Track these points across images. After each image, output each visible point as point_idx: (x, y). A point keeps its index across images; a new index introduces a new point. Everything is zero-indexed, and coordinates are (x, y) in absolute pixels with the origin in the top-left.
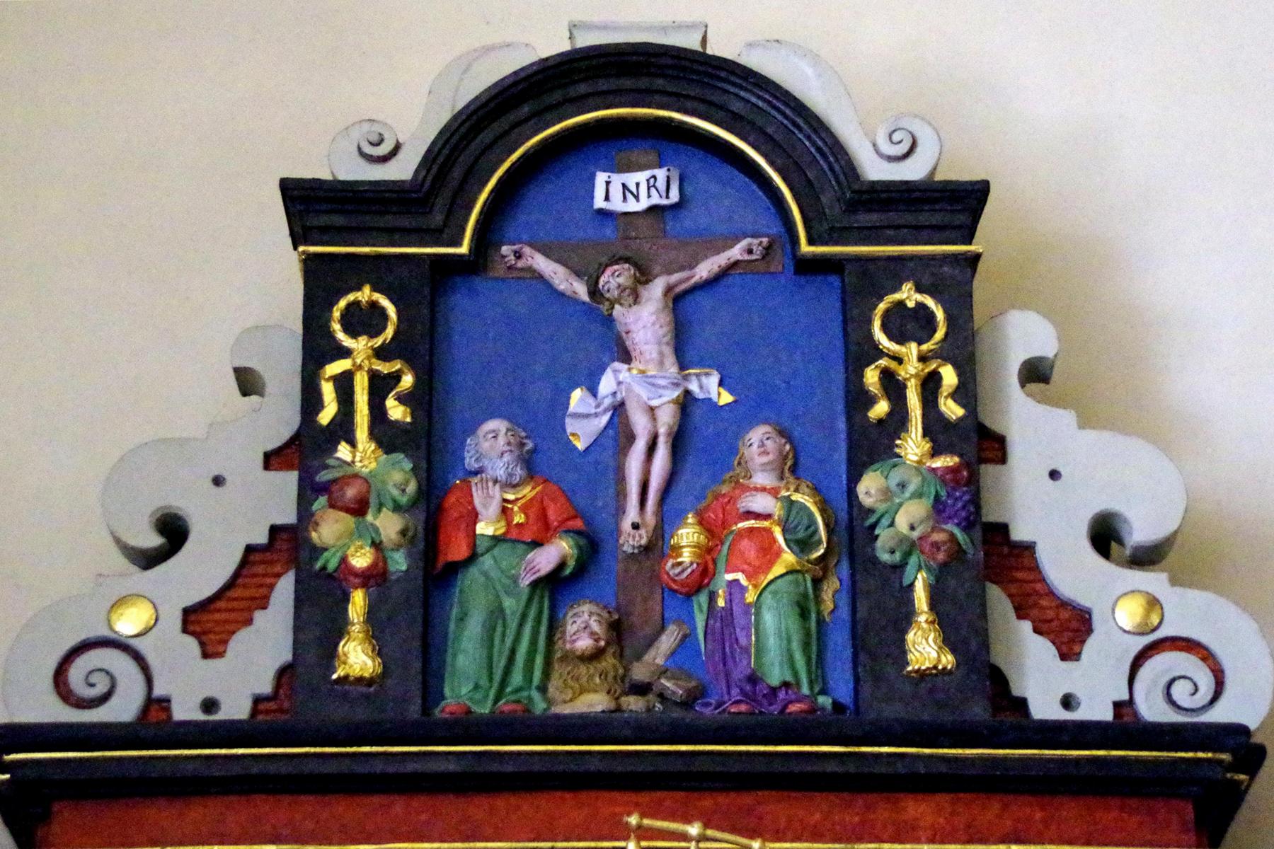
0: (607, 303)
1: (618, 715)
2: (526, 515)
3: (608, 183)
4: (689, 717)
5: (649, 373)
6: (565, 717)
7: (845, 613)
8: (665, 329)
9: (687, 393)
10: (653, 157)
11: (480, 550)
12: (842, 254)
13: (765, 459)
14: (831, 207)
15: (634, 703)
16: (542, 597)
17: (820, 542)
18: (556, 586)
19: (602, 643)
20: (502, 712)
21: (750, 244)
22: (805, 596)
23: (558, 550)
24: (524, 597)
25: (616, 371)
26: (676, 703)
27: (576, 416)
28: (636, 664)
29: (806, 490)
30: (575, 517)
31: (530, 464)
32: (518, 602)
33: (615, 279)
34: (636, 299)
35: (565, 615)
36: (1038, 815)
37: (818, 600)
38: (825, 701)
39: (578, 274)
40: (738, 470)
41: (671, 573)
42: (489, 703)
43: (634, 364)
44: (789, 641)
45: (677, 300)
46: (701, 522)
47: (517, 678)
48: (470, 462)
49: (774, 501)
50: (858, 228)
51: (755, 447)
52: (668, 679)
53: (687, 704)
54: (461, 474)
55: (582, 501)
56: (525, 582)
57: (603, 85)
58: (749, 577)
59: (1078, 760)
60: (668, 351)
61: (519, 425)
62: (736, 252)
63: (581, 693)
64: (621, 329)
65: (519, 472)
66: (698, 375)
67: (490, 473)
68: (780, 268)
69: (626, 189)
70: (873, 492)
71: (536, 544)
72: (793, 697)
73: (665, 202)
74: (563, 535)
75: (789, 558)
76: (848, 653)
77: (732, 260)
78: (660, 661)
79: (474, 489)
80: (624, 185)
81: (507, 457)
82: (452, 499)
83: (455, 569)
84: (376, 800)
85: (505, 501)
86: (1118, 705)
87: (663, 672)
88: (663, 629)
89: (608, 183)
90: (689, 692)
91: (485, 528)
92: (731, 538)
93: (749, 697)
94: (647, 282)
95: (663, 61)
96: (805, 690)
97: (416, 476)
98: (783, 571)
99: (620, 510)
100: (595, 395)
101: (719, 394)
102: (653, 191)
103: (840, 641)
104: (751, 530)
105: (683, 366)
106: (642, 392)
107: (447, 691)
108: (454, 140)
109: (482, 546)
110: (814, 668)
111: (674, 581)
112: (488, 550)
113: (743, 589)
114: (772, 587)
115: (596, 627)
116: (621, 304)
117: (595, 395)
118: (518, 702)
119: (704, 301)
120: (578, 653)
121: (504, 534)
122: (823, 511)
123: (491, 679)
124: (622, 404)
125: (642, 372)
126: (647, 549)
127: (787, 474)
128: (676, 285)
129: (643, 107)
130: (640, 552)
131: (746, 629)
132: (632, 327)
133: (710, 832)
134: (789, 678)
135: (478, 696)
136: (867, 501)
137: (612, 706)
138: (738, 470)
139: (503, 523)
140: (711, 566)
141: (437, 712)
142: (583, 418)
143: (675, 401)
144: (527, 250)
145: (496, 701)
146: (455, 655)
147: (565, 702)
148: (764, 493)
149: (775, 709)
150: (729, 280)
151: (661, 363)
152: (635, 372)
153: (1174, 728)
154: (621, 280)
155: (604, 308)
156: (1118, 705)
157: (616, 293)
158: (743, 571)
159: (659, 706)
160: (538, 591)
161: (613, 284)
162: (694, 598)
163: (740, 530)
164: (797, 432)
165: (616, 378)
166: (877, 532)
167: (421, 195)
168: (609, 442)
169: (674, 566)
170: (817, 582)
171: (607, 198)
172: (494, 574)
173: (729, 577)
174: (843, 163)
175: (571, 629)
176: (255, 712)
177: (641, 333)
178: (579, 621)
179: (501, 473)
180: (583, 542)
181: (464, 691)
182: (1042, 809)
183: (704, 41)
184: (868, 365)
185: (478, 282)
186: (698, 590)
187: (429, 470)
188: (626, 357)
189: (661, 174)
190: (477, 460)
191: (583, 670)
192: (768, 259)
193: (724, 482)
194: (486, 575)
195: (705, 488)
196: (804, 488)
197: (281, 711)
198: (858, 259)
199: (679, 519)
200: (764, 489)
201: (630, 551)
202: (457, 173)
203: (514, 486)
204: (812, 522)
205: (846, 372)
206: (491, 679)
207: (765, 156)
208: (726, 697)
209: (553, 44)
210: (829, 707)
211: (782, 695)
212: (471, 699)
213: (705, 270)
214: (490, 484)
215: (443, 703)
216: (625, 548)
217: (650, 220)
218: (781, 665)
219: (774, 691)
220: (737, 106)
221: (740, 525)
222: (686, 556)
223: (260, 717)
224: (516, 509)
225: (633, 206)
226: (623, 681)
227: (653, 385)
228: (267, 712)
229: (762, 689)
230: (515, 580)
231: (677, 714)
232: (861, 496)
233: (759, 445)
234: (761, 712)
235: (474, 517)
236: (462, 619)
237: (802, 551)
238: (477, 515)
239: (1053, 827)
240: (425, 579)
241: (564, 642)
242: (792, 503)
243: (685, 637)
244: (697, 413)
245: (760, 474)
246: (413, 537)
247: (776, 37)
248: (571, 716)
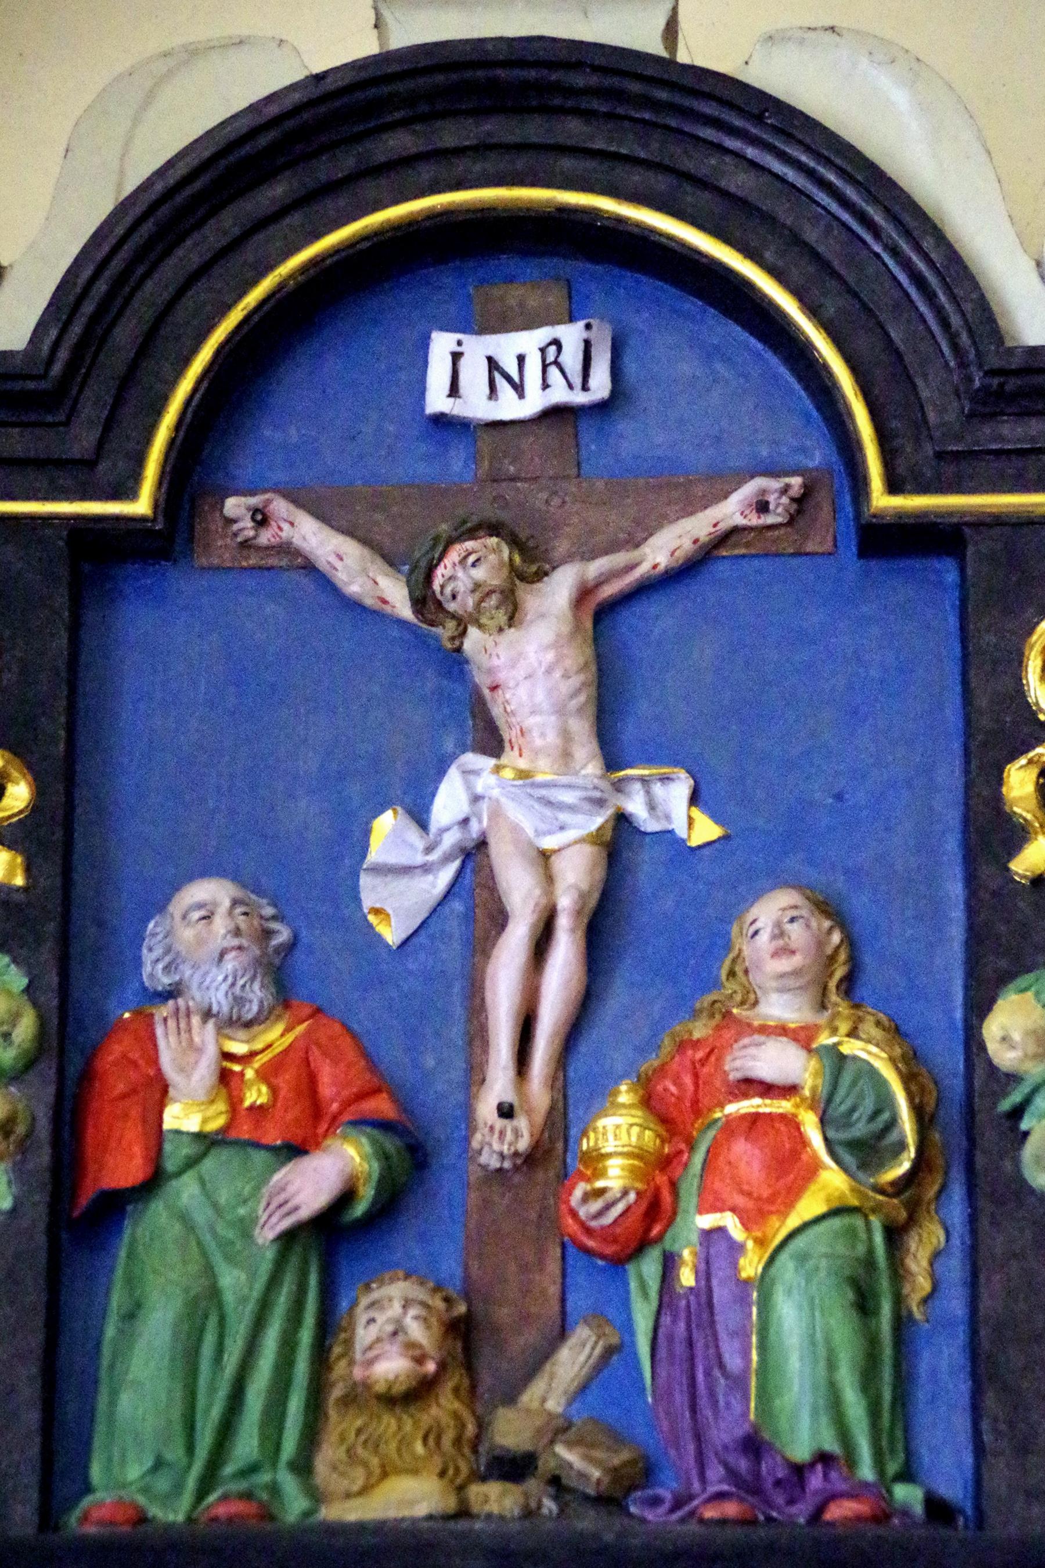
0: (451, 624)
1: (462, 1525)
2: (274, 1091)
3: (456, 356)
5: (540, 778)
7: (956, 1304)
8: (576, 681)
9: (622, 819)
10: (556, 297)
11: (170, 1165)
12: (962, 512)
13: (785, 965)
14: (942, 410)
15: (497, 1499)
16: (305, 1262)
17: (901, 1146)
18: (335, 1242)
19: (431, 1367)
20: (215, 1519)
21: (764, 492)
22: (869, 1262)
23: (341, 1163)
24: (265, 1268)
25: (467, 773)
26: (586, 1497)
27: (381, 870)
28: (501, 1412)
29: (876, 1033)
30: (376, 1091)
31: (282, 975)
32: (252, 1276)
33: (468, 571)
34: (514, 617)
35: (354, 1304)
37: (898, 1272)
38: (908, 1495)
39: (391, 561)
40: (730, 987)
41: (582, 1213)
43: (510, 757)
44: (832, 1365)
45: (603, 616)
46: (648, 1101)
47: (247, 1444)
48: (154, 972)
49: (802, 1054)
50: (998, 453)
51: (764, 937)
52: (570, 1445)
53: (609, 1501)
54: (130, 994)
55: (392, 1054)
56: (267, 1234)
57: (450, 134)
58: (746, 1225)
60: (582, 728)
61: (258, 891)
62: (732, 510)
63: (385, 1475)
64: (482, 681)
65: (257, 995)
66: (644, 781)
67: (195, 997)
68: (828, 546)
69: (499, 369)
70: (1017, 1036)
71: (294, 1150)
72: (843, 1487)
73: (579, 398)
74: (351, 1131)
75: (833, 1181)
76: (964, 1387)
77: (723, 526)
78: (555, 1405)
79: (159, 1031)
80: (492, 364)
81: (230, 964)
82: (114, 1051)
83: (115, 1207)
85: (228, 1056)
87: (561, 1429)
88: (562, 1333)
89: (456, 356)
90: (615, 1473)
91: (183, 1117)
92: (711, 1134)
93: (749, 1487)
94: (541, 575)
95: (579, 80)
96: (866, 1472)
97: (35, 1004)
98: (820, 1209)
99: (475, 1075)
100: (423, 825)
101: (691, 821)
102: (554, 372)
103: (943, 1361)
104: (755, 1118)
105: (612, 762)
106: (523, 817)
107: (96, 1472)
108: (116, 265)
109: (174, 1155)
110: (886, 1416)
111: (589, 1231)
112: (191, 1163)
113: (736, 1249)
114: (799, 1243)
115: (416, 1331)
116: (480, 626)
117: (423, 825)
118: (247, 1496)
119: (661, 617)
120: (380, 1388)
121: (225, 1129)
122: (908, 1079)
123: (190, 1449)
124: (482, 844)
125: (523, 775)
126: (532, 1160)
127: (834, 998)
128: (599, 584)
129: (533, 185)
130: (516, 1168)
131: (742, 1334)
132: (502, 676)
134: (830, 1444)
135: (162, 1483)
136: (1005, 1057)
137: (451, 1504)
138: (730, 987)
139: (221, 1106)
140: (666, 1196)
141: (73, 1519)
142: (399, 877)
143: (595, 839)
144: (280, 507)
145: (201, 1494)
146: (114, 1394)
147: (348, 1496)
148: (783, 1037)
149: (800, 1513)
150: (721, 569)
151: (566, 755)
152: (508, 774)
154: (479, 574)
155: (445, 632)
157: (470, 602)
158: (733, 1210)
159: (549, 1505)
160: (298, 1249)
161: (463, 582)
162: (631, 1268)
163: (729, 1120)
164: (860, 905)
165: (469, 787)
166: (1024, 1126)
167: (44, 385)
168: (454, 926)
169: (586, 1198)
170: (895, 1235)
171: (454, 390)
172: (201, 1216)
173: (706, 1221)
174: (968, 307)
175: (364, 1336)
177: (522, 692)
178: (381, 1318)
179: (219, 999)
180: (391, 1144)
181: (134, 1472)
183: (671, 31)
184: (1012, 758)
185: (180, 583)
186: (641, 1246)
187: (64, 989)
188: (492, 742)
189: (571, 335)
190: (167, 969)
191: (388, 1423)
192: (801, 522)
193: (695, 1014)
194: (184, 1218)
195: (657, 1030)
196: (869, 1028)
198: (996, 521)
199: (600, 1095)
200: (782, 1030)
201: (495, 1163)
202: (126, 334)
203: (248, 1025)
204: (884, 1102)
205: (967, 772)
206: (190, 1449)
207: (798, 293)
208: (696, 1486)
209: (339, 38)
210: (918, 1509)
211: (815, 1481)
212: (145, 1490)
213: (661, 551)
214: (196, 1020)
215: (87, 1501)
216: (483, 1159)
217: (548, 437)
218: (815, 1413)
219: (799, 1471)
220: (739, 182)
221: (731, 1108)
222: (615, 1176)
224: (250, 1074)
225: (511, 408)
226: (475, 1450)
227: (549, 803)
229: (770, 1469)
230: (245, 1228)
231: (587, 1521)
232: (992, 1047)
233: (774, 931)
234: (769, 1519)
235: (159, 1091)
236: (131, 1315)
237: (864, 1165)
238: (165, 1089)
240: (52, 1232)
241: (352, 1363)
242: (843, 1057)
243: (609, 1352)
244: (646, 868)
245: (774, 997)
246: (29, 1134)
247: (828, 23)
248: (361, 1527)
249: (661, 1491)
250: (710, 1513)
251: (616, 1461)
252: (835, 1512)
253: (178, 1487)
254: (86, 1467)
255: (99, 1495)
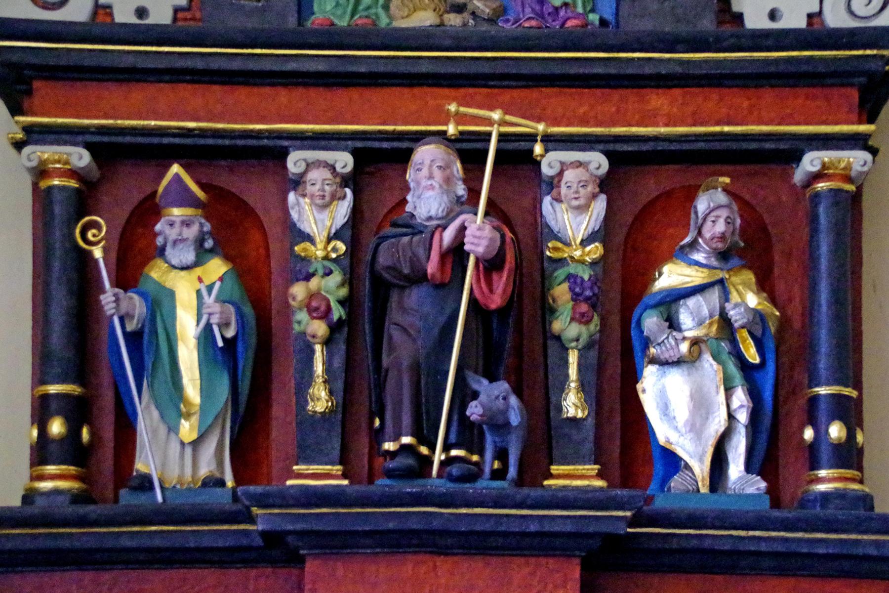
1: (442, 28)
4: (492, 30)
6: (403, 29)
15: (454, 20)
36: (746, 104)
38: (594, 18)
42: (347, 17)
53: (491, 21)
59: (777, 61)
84: (267, 90)
86: (810, 16)
96: (580, 10)
133: (508, 118)
135: (339, 12)
145: (353, 15)
147: (403, 18)
149: (557, 25)
153: (852, 32)
156: (810, 16)
159: (471, 22)
176: (175, 19)
181: (329, 7)
182: (749, 99)
197: (193, 19)
208: (521, 16)
210: (597, 23)
211: (562, 13)
212: (333, 14)
215: (313, 17)
219: (557, 9)
223: (180, 23)
228: (185, 19)
231: (485, 27)
239: (755, 113)
248: (407, 29)
249: (509, 17)
250: (526, 25)
251: (494, 6)
252: (569, 24)
253: (345, 13)
254: (312, 6)
255: (430, 481)
